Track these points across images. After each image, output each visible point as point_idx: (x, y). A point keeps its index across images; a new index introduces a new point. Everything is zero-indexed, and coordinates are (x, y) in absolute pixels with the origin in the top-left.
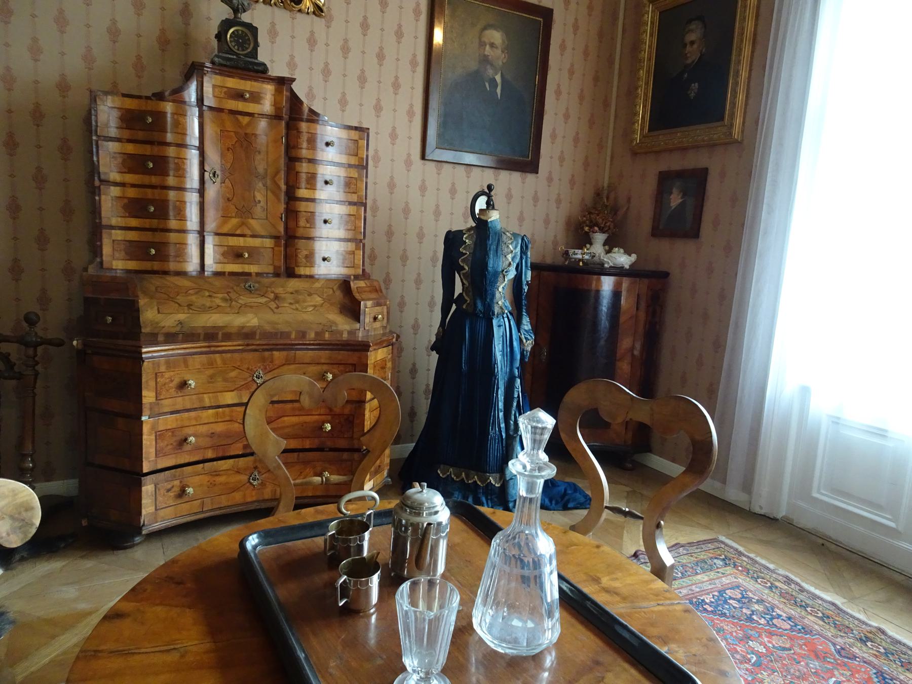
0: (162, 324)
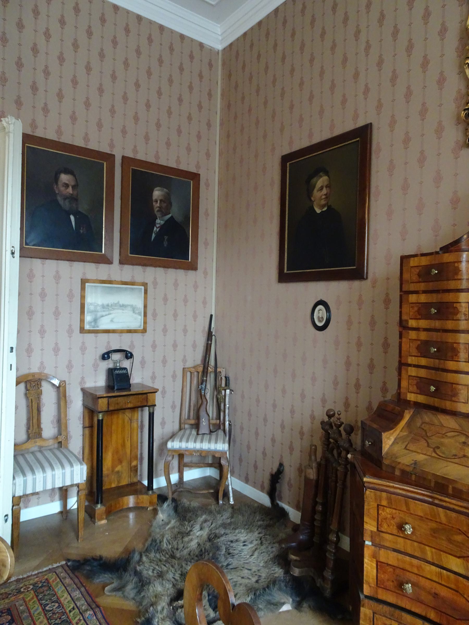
0: (399, 460)
